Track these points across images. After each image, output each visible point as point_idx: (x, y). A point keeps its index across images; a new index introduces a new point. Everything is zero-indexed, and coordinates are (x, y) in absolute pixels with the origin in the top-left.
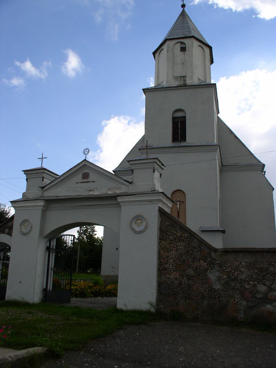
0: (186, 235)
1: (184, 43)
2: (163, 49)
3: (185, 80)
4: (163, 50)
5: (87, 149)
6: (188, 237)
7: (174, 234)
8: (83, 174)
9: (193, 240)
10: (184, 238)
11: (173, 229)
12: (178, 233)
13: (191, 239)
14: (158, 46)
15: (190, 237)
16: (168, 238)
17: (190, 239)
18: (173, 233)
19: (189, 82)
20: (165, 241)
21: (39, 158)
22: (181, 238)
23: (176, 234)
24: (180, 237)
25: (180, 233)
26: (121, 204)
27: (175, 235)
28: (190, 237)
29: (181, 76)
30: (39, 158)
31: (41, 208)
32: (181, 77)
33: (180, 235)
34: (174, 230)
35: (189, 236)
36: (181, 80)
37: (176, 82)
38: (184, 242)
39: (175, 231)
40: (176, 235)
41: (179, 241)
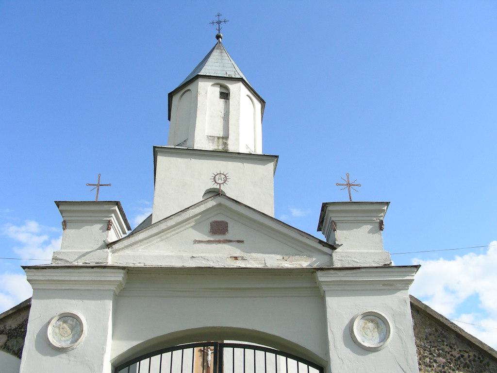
0: (471, 354)
1: (227, 88)
2: (189, 90)
3: (225, 144)
4: (188, 92)
5: (223, 174)
6: (477, 359)
7: (447, 351)
8: (211, 224)
9: (488, 364)
10: (467, 361)
11: (443, 341)
12: (455, 350)
13: (484, 362)
14: (177, 86)
15: (481, 359)
16: (435, 361)
17: (481, 362)
18: (443, 350)
19: (231, 148)
20: (430, 366)
21: (90, 185)
22: (462, 359)
23: (451, 353)
24: (459, 358)
25: (458, 350)
26: (324, 288)
27: (449, 353)
28: (481, 359)
29: (218, 136)
30: (90, 185)
31: (113, 288)
32: (219, 138)
33: (459, 355)
34: (445, 343)
35: (477, 355)
36: (218, 142)
37: (211, 144)
38: (470, 369)
39: (447, 345)
40: (452, 355)
41: (458, 366)
